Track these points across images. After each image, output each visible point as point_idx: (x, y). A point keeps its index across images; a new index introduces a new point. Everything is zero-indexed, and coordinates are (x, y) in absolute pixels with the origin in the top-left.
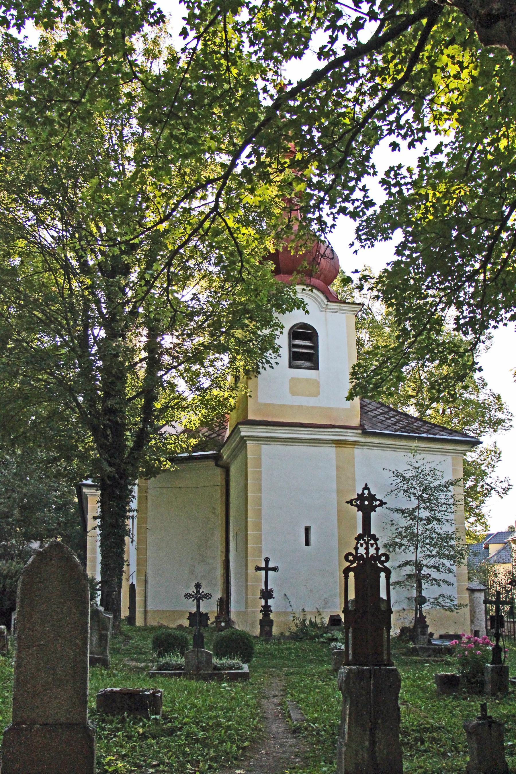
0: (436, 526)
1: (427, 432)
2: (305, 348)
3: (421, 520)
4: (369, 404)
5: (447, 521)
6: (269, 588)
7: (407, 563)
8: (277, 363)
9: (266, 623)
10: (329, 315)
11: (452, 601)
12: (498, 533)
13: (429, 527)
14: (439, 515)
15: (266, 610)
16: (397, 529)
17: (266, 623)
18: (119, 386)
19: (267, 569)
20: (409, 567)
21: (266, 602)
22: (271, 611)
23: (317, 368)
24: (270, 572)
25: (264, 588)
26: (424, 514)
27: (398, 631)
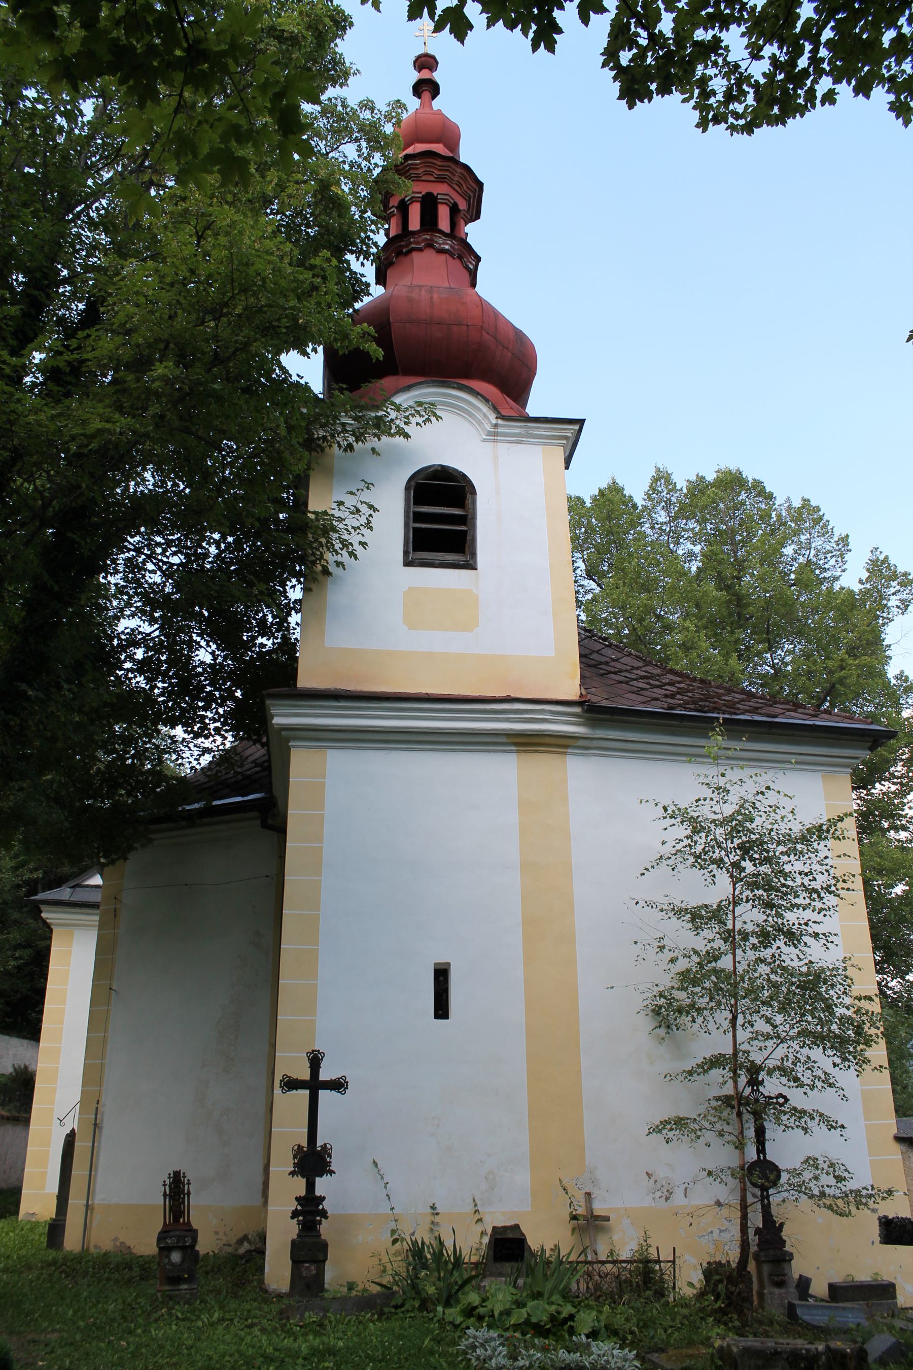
0: (785, 949)
1: (755, 710)
2: (442, 519)
3: (745, 936)
4: (617, 660)
5: (816, 935)
6: (320, 1143)
7: (715, 1062)
8: (363, 544)
9: (310, 1250)
10: (503, 447)
11: (839, 1179)
12: (467, 168)
13: (767, 953)
14: (791, 917)
15: (310, 1210)
16: (673, 961)
17: (310, 1250)
18: (893, 1057)
19: (314, 1085)
20: (717, 1074)
21: (311, 1186)
22: (324, 1214)
23: (470, 566)
24: (323, 1094)
25: (304, 1143)
26: (749, 916)
27: (697, 1278)
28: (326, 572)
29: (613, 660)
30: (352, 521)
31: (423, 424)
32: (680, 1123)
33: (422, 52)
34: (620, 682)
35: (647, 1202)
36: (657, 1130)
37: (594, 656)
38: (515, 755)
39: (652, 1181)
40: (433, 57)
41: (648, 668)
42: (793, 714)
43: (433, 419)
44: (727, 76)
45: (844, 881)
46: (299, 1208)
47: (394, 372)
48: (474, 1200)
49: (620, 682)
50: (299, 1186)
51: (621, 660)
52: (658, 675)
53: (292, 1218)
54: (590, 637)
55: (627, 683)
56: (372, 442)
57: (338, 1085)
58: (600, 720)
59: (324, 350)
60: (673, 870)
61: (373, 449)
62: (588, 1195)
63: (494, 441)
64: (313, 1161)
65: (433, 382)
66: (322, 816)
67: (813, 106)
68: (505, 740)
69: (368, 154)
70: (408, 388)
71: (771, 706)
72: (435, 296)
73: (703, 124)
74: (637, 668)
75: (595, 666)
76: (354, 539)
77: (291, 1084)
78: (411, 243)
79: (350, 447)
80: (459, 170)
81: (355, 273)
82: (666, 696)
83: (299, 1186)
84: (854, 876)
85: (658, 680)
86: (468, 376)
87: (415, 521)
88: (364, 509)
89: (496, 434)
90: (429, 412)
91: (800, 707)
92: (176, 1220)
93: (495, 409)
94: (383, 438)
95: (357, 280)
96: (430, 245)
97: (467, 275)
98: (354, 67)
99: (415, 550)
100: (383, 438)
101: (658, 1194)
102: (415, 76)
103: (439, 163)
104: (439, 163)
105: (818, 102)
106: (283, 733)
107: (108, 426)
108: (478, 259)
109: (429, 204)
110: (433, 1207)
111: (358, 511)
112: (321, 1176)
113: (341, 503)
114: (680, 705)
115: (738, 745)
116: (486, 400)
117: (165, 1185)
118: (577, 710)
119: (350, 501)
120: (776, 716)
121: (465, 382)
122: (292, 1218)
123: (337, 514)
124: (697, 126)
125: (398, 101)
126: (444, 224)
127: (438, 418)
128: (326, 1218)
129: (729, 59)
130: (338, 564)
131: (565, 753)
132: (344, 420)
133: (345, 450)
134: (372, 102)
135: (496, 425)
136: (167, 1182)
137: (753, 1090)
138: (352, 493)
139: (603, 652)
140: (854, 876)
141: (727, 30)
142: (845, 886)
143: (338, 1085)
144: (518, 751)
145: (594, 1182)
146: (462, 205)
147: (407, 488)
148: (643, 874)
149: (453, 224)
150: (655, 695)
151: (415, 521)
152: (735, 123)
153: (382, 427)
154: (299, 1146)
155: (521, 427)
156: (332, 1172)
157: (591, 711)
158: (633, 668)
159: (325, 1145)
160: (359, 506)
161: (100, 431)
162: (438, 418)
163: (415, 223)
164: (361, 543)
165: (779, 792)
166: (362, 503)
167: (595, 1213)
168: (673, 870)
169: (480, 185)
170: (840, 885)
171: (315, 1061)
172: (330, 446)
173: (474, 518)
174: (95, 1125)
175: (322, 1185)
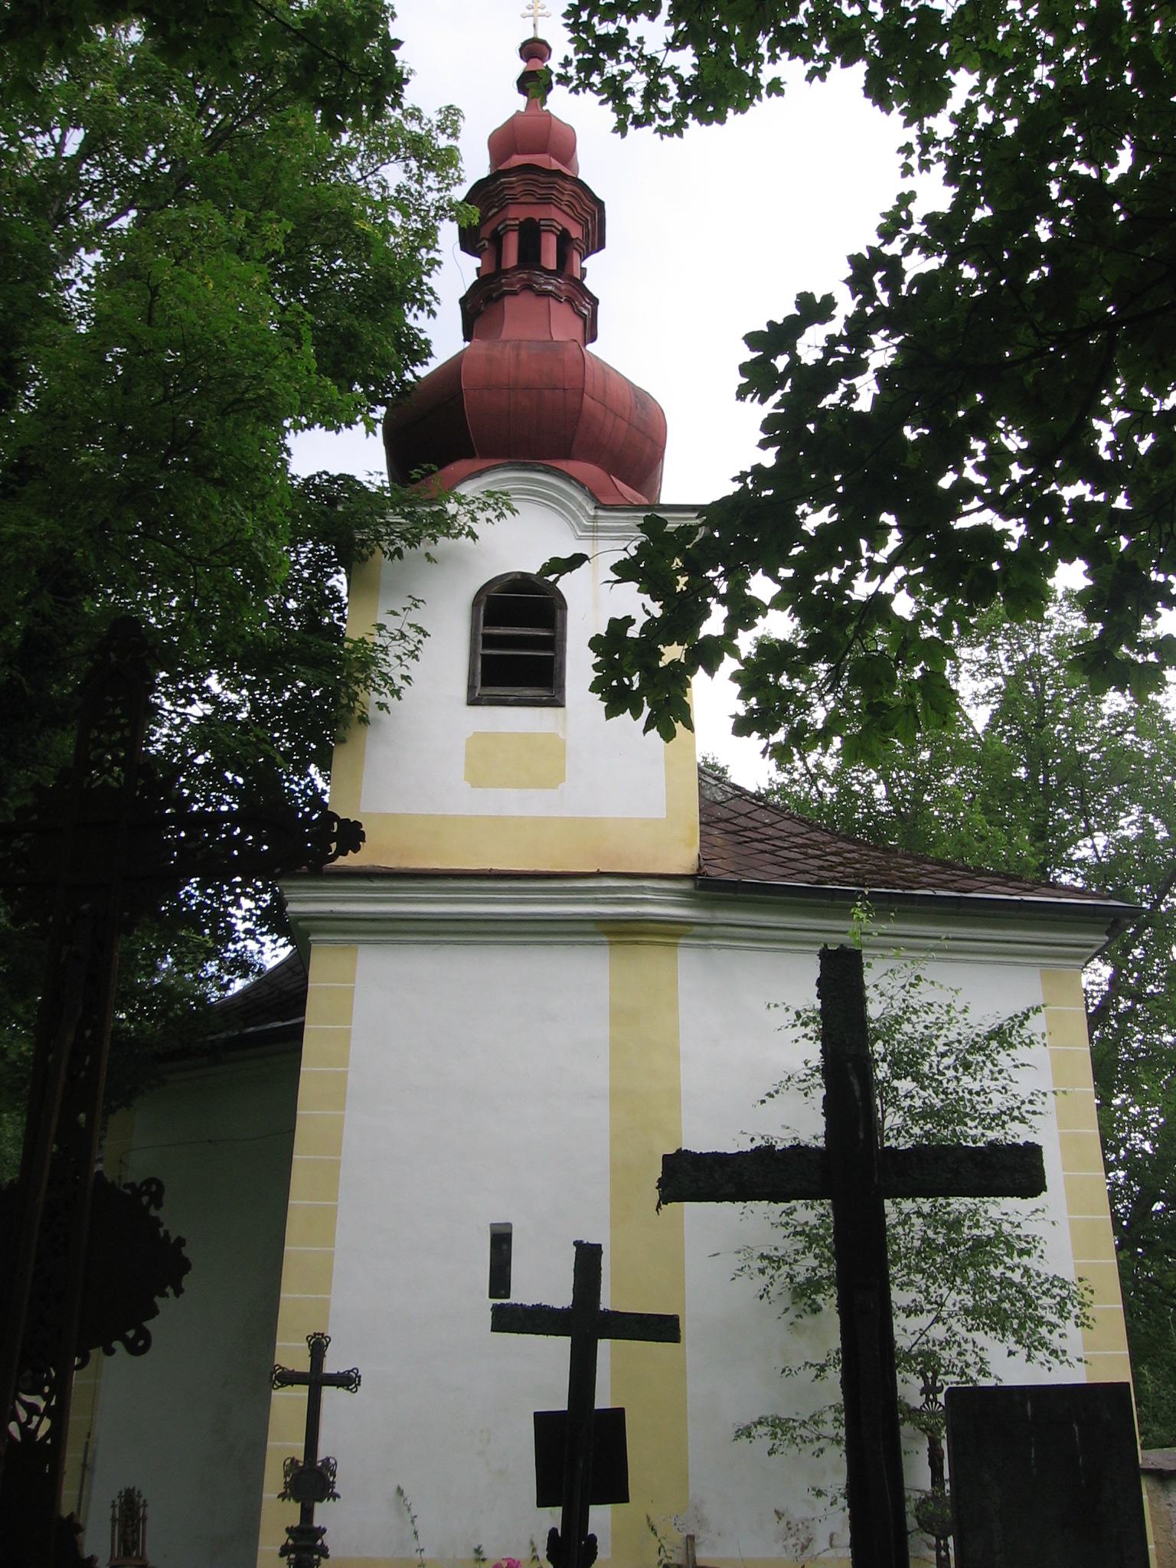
4: (770, 825)
6: (321, 1456)
8: (406, 678)
19: (316, 1380)
21: (307, 1514)
24: (328, 1393)
25: (300, 1457)
28: (364, 720)
29: (766, 825)
30: (396, 648)
31: (495, 521)
32: (778, 1426)
33: (531, 36)
34: (762, 852)
35: (776, 1551)
36: (745, 1432)
37: (742, 821)
38: (606, 949)
39: (783, 1523)
40: (544, 43)
41: (812, 835)
42: (998, 888)
43: (507, 513)
44: (645, 70)
45: (1031, 1102)
46: (291, 1542)
47: (470, 455)
48: (532, 1543)
49: (762, 852)
50: (291, 1512)
51: (777, 826)
52: (823, 843)
53: (282, 1555)
54: (740, 797)
55: (772, 853)
56: (426, 545)
57: (348, 1381)
58: (720, 899)
59: (384, 429)
60: (806, 1095)
61: (427, 555)
62: (691, 1538)
63: (593, 538)
64: (312, 1481)
65: (511, 464)
66: (349, 1031)
67: (760, 98)
68: (590, 927)
69: (420, 175)
70: (479, 473)
71: (972, 878)
72: (523, 354)
73: (621, 129)
74: (796, 835)
75: (735, 833)
76: (396, 673)
77: (290, 1378)
78: (502, 285)
79: (399, 552)
80: (568, 187)
81: (412, 328)
82: (821, 868)
83: (291, 1512)
84: (1045, 1094)
85: (820, 849)
86: (567, 456)
87: (484, 647)
88: (411, 633)
89: (596, 529)
90: (499, 503)
91: (1014, 880)
92: (127, 1552)
93: (593, 496)
94: (442, 540)
95: (416, 336)
96: (528, 287)
97: (580, 323)
98: (407, 66)
99: (484, 684)
100: (442, 540)
101: (792, 1541)
102: (520, 66)
103: (542, 179)
104: (542, 179)
105: (763, 91)
106: (300, 924)
107: (24, 530)
108: (595, 302)
109: (531, 234)
110: (478, 1551)
111: (403, 636)
112: (321, 1501)
113: (381, 627)
114: (835, 879)
115: (884, 927)
116: (581, 485)
117: (113, 1506)
118: (686, 886)
119: (393, 624)
120: (971, 891)
121: (562, 465)
122: (282, 1555)
123: (379, 641)
124: (615, 130)
125: (450, 107)
126: (550, 261)
127: (514, 511)
128: (327, 1557)
129: (645, 52)
130: (382, 706)
131: (676, 945)
132: (392, 519)
133: (392, 558)
134: (418, 110)
135: (595, 517)
136: (117, 1502)
137: (927, 1400)
138: (394, 613)
139: (754, 815)
140: (1045, 1094)
141: (636, 20)
142: (1031, 1108)
143: (348, 1381)
144: (611, 943)
145: (701, 1522)
146: (576, 232)
147: (476, 604)
148: (763, 1102)
149: (563, 258)
150: (807, 867)
151: (484, 647)
152: (664, 124)
153: (442, 524)
154: (293, 1459)
155: (628, 518)
156: (335, 1496)
157: (705, 886)
158: (791, 834)
159: (328, 1459)
160: (406, 629)
161: (16, 537)
162: (514, 511)
163: (511, 258)
164: (404, 677)
165: (932, 983)
166: (411, 626)
167: (699, 1564)
168: (806, 1095)
169: (600, 204)
170: (1027, 1107)
171: (318, 1346)
172: (372, 553)
173: (563, 639)
174: (84, 1466)
175: (323, 1514)
